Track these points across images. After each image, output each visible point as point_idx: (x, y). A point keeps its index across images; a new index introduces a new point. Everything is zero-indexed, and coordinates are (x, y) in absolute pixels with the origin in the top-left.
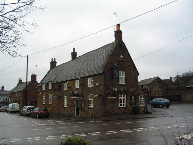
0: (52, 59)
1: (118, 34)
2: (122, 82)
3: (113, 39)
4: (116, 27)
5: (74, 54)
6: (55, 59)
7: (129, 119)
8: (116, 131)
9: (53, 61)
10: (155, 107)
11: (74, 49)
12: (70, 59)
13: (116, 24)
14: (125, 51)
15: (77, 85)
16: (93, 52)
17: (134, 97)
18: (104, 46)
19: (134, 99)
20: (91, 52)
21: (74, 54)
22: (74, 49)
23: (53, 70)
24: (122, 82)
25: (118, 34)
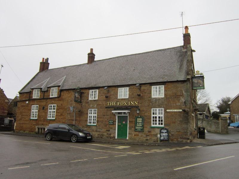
0: (43, 59)
1: (187, 37)
2: (35, 109)
3: (181, 43)
4: (184, 30)
5: (91, 56)
6: (48, 59)
7: (156, 145)
8: (174, 171)
9: (44, 61)
10: (64, 128)
11: (92, 50)
12: (86, 61)
13: (184, 26)
14: (5, 97)
15: (123, 93)
16: (117, 59)
17: (141, 119)
18: (158, 51)
19: (141, 121)
20: (107, 59)
21: (91, 56)
22: (92, 50)
23: (41, 74)
24: (35, 109)
25: (187, 37)
